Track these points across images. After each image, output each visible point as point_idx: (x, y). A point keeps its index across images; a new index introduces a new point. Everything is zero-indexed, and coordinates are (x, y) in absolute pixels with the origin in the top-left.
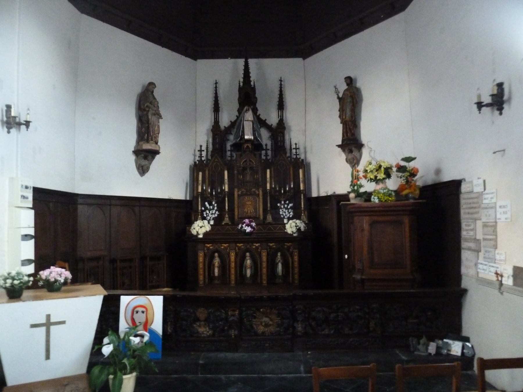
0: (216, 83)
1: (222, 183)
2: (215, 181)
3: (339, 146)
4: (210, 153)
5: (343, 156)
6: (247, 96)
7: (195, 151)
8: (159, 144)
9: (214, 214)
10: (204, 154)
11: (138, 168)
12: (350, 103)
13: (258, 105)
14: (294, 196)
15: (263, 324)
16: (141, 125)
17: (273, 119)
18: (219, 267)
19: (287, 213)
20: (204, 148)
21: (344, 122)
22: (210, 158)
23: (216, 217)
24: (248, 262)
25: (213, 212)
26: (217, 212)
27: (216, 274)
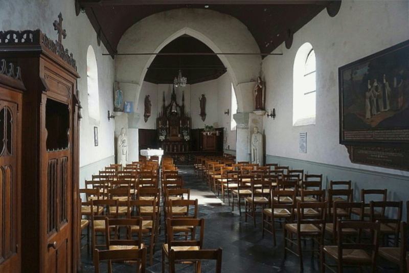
1: (166, 125)
5: (201, 117)
6: (174, 97)
12: (203, 101)
17: (181, 104)
21: (201, 108)
24: (175, 148)
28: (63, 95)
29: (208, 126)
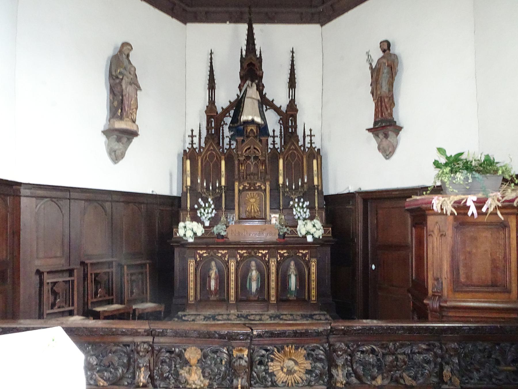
0: (211, 54)
2: (211, 172)
3: (369, 130)
4: (203, 140)
6: (251, 69)
7: (184, 136)
8: (137, 123)
9: (211, 213)
10: (196, 140)
11: (110, 154)
12: (385, 71)
13: (264, 81)
14: (309, 192)
15: (285, 370)
16: (113, 98)
17: (281, 100)
18: (216, 279)
19: (302, 213)
20: (196, 133)
22: (203, 145)
23: (212, 217)
25: (210, 211)
26: (214, 211)
27: (213, 288)
28: (316, 314)
29: (457, 158)
